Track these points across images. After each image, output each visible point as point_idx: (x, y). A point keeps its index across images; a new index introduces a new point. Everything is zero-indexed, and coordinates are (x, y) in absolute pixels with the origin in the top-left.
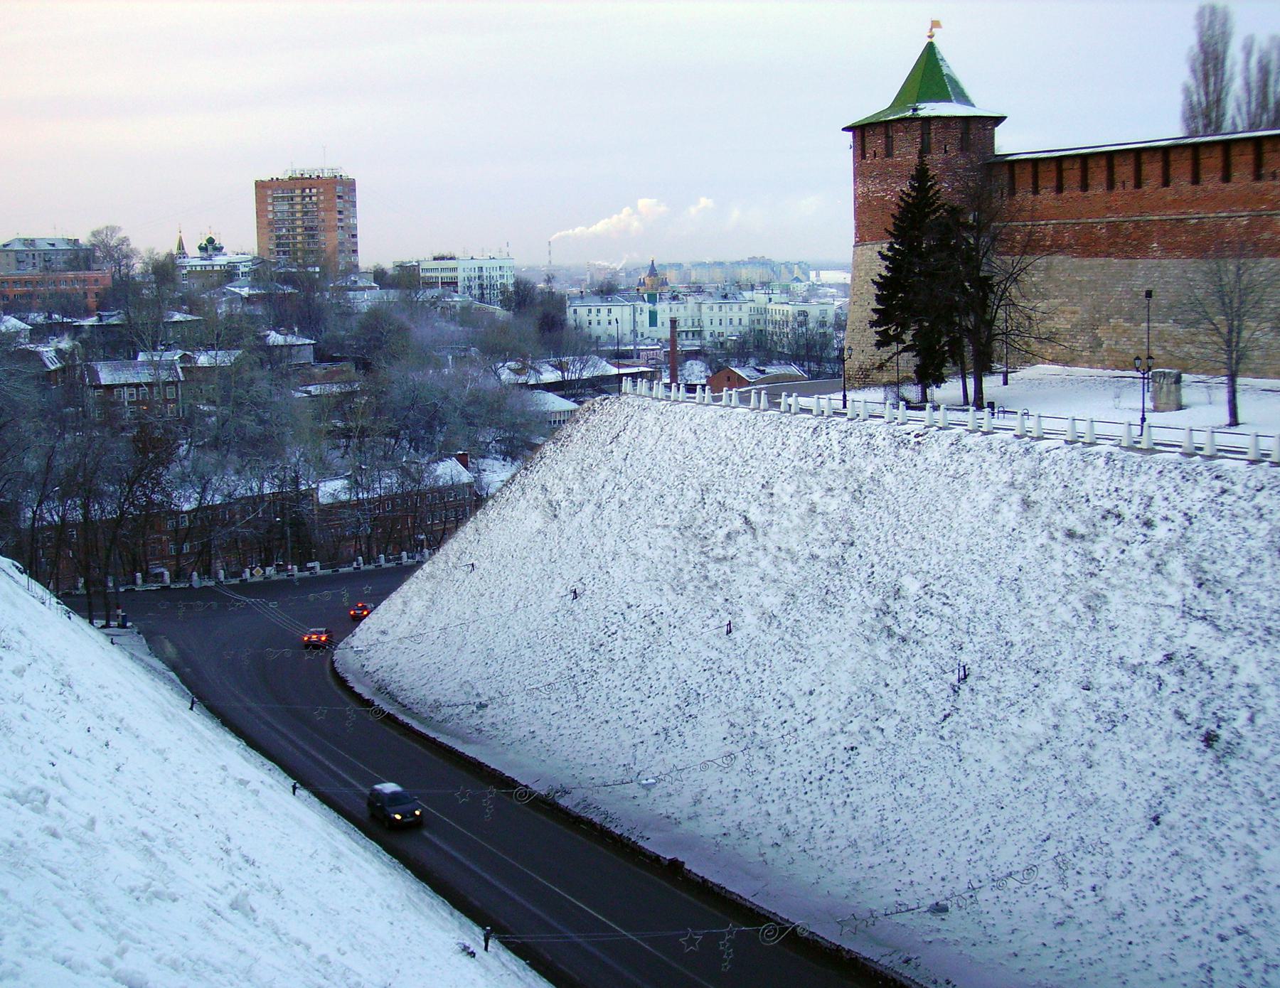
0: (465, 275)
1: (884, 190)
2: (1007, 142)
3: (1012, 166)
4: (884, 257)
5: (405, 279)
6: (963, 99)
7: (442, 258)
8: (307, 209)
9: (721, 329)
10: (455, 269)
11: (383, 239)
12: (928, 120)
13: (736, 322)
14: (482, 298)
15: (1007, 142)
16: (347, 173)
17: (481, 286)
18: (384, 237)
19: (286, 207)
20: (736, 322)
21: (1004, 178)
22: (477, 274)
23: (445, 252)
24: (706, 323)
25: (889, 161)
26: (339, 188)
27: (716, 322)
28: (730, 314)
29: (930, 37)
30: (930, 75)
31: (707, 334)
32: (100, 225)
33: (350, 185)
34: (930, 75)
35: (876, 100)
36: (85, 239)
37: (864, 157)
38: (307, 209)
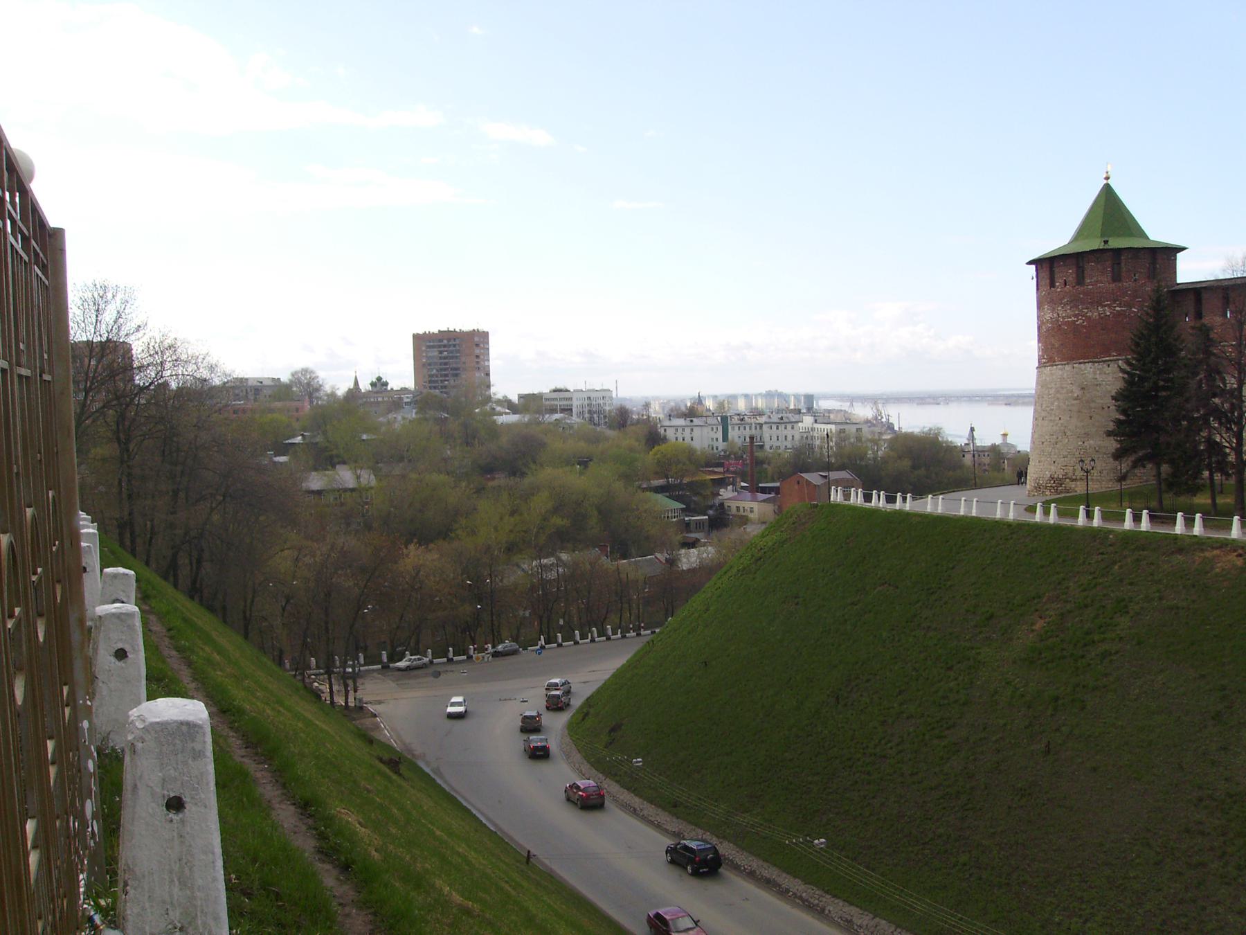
0: (579, 403)
1: (1075, 316)
2: (1188, 271)
3: (1198, 292)
4: (1122, 371)
5: (530, 403)
6: (1142, 234)
7: (560, 390)
8: (451, 358)
9: (778, 444)
10: (570, 399)
11: (511, 375)
12: (1118, 252)
13: (790, 438)
14: (591, 419)
15: (1188, 271)
16: (483, 327)
17: (590, 412)
18: (511, 375)
19: (436, 353)
20: (790, 438)
21: (1189, 305)
22: (586, 402)
23: (560, 386)
24: (766, 439)
25: (1081, 289)
26: (476, 339)
27: (774, 438)
28: (785, 432)
29: (1107, 178)
30: (1109, 210)
31: (767, 447)
32: (298, 365)
33: (485, 336)
34: (1109, 210)
35: (1059, 232)
36: (285, 378)
37: (1052, 285)
38: (451, 358)
